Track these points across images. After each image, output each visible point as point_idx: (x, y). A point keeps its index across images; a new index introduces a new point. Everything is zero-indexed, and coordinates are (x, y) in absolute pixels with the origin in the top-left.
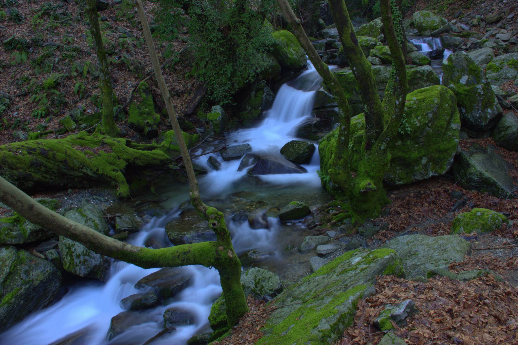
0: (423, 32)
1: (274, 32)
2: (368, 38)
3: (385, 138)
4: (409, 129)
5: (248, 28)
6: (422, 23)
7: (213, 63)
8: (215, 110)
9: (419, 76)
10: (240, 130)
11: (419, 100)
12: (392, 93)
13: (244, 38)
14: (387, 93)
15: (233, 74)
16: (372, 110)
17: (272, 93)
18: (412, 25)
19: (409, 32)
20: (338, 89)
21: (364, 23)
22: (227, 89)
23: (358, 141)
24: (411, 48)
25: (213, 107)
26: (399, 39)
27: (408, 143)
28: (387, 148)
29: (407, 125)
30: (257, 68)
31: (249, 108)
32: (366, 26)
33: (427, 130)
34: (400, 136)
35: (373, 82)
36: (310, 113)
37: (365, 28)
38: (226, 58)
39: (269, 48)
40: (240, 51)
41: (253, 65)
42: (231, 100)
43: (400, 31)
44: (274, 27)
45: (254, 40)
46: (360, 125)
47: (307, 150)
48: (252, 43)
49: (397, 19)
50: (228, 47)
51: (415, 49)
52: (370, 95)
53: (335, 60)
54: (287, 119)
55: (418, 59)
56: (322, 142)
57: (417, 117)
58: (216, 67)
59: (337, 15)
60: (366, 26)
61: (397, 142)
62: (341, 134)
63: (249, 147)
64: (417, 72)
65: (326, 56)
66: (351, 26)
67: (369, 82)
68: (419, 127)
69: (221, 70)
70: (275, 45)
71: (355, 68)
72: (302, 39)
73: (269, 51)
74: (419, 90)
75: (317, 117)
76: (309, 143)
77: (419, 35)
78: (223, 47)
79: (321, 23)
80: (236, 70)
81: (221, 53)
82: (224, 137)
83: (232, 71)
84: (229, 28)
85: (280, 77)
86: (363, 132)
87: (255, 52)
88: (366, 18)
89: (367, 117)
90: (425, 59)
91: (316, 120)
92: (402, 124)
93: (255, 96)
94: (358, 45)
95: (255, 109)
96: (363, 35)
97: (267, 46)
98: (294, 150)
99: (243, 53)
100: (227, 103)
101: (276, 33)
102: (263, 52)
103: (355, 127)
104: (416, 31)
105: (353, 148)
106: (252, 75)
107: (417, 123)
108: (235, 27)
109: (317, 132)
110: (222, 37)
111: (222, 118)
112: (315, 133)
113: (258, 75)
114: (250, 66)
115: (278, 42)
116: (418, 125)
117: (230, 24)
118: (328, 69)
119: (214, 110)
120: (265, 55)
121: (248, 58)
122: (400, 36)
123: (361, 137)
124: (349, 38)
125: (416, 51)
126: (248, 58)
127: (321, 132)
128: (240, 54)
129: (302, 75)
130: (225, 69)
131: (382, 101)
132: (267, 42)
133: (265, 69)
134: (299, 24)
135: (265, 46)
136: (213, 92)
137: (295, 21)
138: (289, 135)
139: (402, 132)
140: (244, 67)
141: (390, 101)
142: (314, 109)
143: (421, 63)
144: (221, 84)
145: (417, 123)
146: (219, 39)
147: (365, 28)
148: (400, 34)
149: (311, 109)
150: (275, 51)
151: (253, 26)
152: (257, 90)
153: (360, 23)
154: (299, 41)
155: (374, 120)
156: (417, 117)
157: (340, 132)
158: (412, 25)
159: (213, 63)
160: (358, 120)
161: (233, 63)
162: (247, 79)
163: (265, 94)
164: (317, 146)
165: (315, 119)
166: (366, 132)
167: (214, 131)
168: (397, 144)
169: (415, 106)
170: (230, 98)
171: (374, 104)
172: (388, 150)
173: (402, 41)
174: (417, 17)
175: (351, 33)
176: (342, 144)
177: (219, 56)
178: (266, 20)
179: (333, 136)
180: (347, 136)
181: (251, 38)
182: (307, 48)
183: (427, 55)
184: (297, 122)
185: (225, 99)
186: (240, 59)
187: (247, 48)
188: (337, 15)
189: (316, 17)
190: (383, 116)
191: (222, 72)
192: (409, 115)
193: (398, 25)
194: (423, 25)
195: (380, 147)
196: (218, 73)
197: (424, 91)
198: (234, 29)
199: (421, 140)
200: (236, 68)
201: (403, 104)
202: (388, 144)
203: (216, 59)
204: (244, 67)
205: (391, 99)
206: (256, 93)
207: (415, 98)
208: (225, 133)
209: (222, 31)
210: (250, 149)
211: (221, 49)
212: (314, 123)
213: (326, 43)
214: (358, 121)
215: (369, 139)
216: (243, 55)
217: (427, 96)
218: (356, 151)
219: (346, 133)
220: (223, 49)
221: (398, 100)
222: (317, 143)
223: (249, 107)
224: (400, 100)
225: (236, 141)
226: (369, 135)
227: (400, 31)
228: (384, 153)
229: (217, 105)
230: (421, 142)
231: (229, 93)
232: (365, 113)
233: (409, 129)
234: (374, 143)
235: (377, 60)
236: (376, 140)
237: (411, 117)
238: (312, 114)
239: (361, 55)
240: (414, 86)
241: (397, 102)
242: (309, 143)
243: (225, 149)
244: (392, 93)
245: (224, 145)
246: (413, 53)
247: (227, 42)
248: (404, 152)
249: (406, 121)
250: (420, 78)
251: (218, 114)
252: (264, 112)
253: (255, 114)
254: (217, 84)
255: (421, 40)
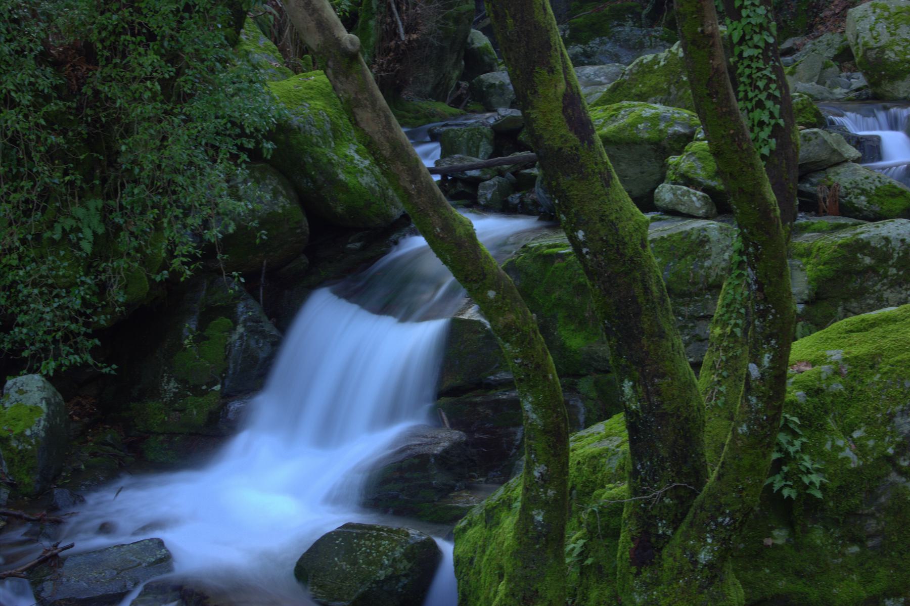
0: (887, 87)
1: (285, 76)
2: (660, 108)
3: (713, 518)
4: (816, 478)
5: (173, 57)
6: (882, 50)
7: (15, 197)
8: (21, 392)
9: (868, 260)
10: (126, 480)
11: (856, 362)
12: (738, 331)
13: (153, 98)
14: (718, 331)
15: (105, 245)
16: (655, 399)
17: (268, 327)
18: (844, 56)
19: (834, 85)
20: (513, 317)
21: (653, 48)
22: (77, 304)
23: (605, 530)
24: (834, 151)
25: (10, 382)
26: (765, 117)
27: (818, 536)
28: (722, 558)
29: (808, 464)
30: (206, 224)
31: (172, 386)
32: (656, 61)
33: (893, 484)
34: (783, 510)
35: (654, 288)
36: (427, 406)
37: (651, 71)
38: (76, 177)
39: (258, 143)
40: (138, 151)
41: (187, 212)
42: (94, 351)
43: (767, 87)
44: (285, 56)
45: (196, 107)
46: (615, 463)
47: (405, 565)
48: (189, 119)
49: (756, 38)
50: (83, 129)
51: (852, 152)
52: (644, 341)
53: (529, 197)
54: (329, 432)
55: (864, 192)
56: (464, 530)
57: (847, 431)
58: (27, 213)
59: (510, 21)
60: (656, 61)
61: (770, 536)
62: (530, 501)
63: (159, 554)
64: (862, 246)
65: (495, 180)
66: (566, 68)
67: (638, 290)
68: (858, 471)
69: (51, 227)
70: (282, 131)
71: (581, 234)
72: (364, 116)
73: (255, 155)
74: (854, 319)
75: (454, 426)
76: (415, 533)
77: (873, 97)
78: (64, 133)
79: (477, 45)
80: (118, 228)
81: (51, 155)
82: (54, 508)
83: (101, 231)
84: (88, 53)
85: (304, 259)
86: (619, 490)
87: (200, 157)
88: (660, 30)
89: (632, 428)
90: (894, 193)
91: (447, 437)
92: (787, 458)
93: (200, 339)
94: (591, 142)
95: (197, 391)
96: (642, 97)
97: (251, 136)
98: (354, 563)
99: (148, 159)
100: (73, 367)
101: (293, 82)
102: (234, 157)
103: (595, 470)
104: (859, 80)
105: (583, 555)
106: (185, 249)
107: (848, 453)
108: (113, 49)
109: (452, 489)
110: (56, 88)
111: (50, 430)
112: (446, 491)
113: (210, 251)
114: (178, 212)
115: (296, 121)
116: (855, 462)
117: (94, 37)
118: (471, 236)
119: (13, 395)
120: (241, 173)
121: (170, 182)
122: (769, 104)
123: (615, 509)
124: (558, 114)
125: (857, 161)
126: (170, 182)
127: (470, 488)
128: (134, 162)
129: (397, 253)
130: (68, 223)
131: (697, 366)
132: (250, 120)
133: (240, 228)
134: (353, 57)
135: (243, 134)
136: (14, 316)
137: (337, 42)
138: (334, 499)
139: (786, 492)
140: (151, 215)
141: (731, 365)
142: (439, 395)
143: (876, 208)
144: (52, 287)
145: (848, 453)
146: (42, 98)
147: (651, 71)
148: (770, 97)
149: (429, 392)
150: (281, 153)
151: (189, 49)
152: (208, 315)
153: (639, 48)
154: (356, 124)
155: (665, 442)
156: (847, 431)
157: (527, 489)
158: (844, 56)
159: (15, 197)
160: (601, 440)
161: (108, 197)
162: (165, 266)
163: (240, 329)
164: (447, 548)
165: (442, 434)
166: (635, 492)
167: (11, 485)
168: (768, 541)
169: (837, 386)
170: (89, 344)
171: (663, 376)
172: (729, 566)
173: (777, 125)
174: (866, 25)
175: (565, 96)
176: (540, 543)
177: (42, 168)
178: (250, 30)
179: (510, 507)
180: (560, 509)
181: (186, 98)
182: (387, 152)
183: (900, 179)
184: (369, 445)
185: (65, 349)
186: (136, 182)
187: (164, 138)
188: (510, 21)
189: (457, 20)
190: (701, 427)
191: (57, 237)
192: (812, 422)
193: (761, 64)
194: (890, 55)
195: (694, 554)
196: (38, 237)
197: (874, 324)
198: (108, 60)
199: (872, 525)
200: (119, 220)
201: (777, 377)
202: (724, 541)
203: (31, 177)
204: (151, 215)
205: (735, 357)
206: (203, 325)
207: (836, 355)
208: (60, 495)
209: (57, 65)
210: (165, 560)
211: (52, 139)
212: (438, 449)
213: (494, 128)
214: (606, 444)
215: (646, 521)
216: (148, 167)
217: (886, 343)
218: (598, 567)
219: (551, 493)
220: (61, 140)
221: (756, 359)
222: (448, 538)
223: (172, 384)
224: (766, 360)
225: (105, 529)
226: (648, 502)
227: (767, 87)
228: (711, 581)
229: (32, 371)
230: (870, 536)
231: (86, 324)
232: (629, 413)
233: (816, 478)
234: (666, 539)
235: (695, 199)
236: (675, 523)
237: (822, 428)
238: (434, 414)
239: (607, 181)
240: (846, 300)
241: (754, 370)
242: (415, 533)
243: (52, 561)
244: (738, 331)
245: (47, 544)
246: (841, 169)
247: (79, 109)
248: (799, 574)
249: (804, 448)
250: (871, 269)
251: (34, 409)
252: (234, 406)
253: (196, 411)
254: (35, 284)
255: (881, 116)
